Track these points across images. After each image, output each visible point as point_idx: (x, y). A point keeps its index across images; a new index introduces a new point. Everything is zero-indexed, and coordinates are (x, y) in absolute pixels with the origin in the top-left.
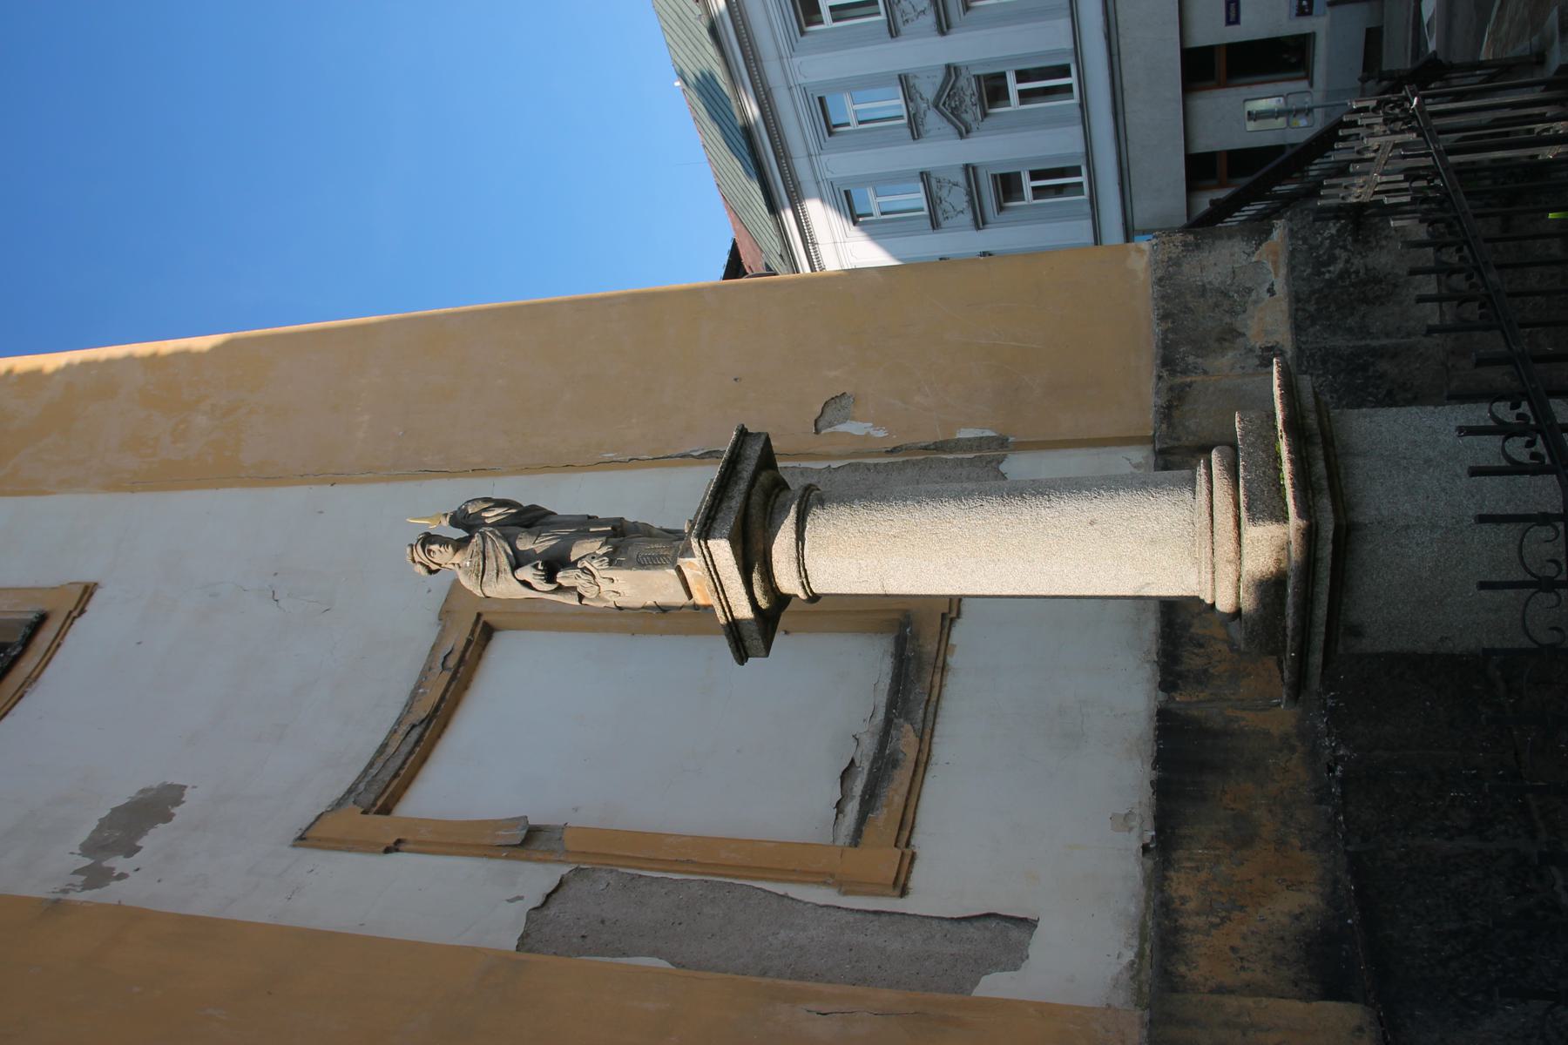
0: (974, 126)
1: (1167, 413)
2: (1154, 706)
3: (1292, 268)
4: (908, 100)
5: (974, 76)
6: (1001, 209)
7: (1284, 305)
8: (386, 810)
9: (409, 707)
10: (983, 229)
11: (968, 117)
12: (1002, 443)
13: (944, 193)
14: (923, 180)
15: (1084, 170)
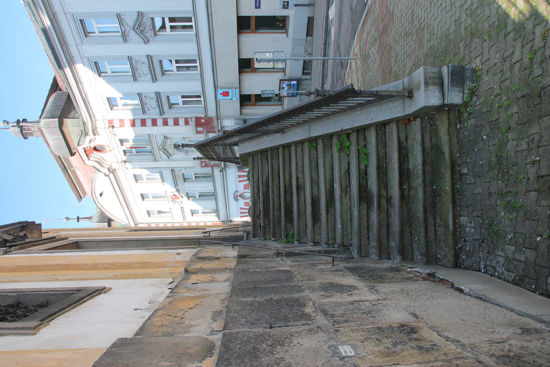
0: (151, 39)
4: (121, 26)
5: (150, 18)
11: (148, 35)
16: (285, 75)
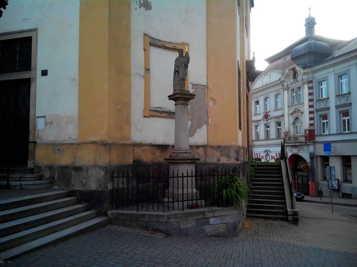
1: (211, 146)
2: (170, 144)
3: (231, 163)
6: (340, 112)
7: (226, 162)
8: (150, 45)
9: (167, 42)
10: (335, 108)
12: (208, 125)
13: (345, 98)
14: (349, 93)
15: (349, 132)
16: (342, 182)
